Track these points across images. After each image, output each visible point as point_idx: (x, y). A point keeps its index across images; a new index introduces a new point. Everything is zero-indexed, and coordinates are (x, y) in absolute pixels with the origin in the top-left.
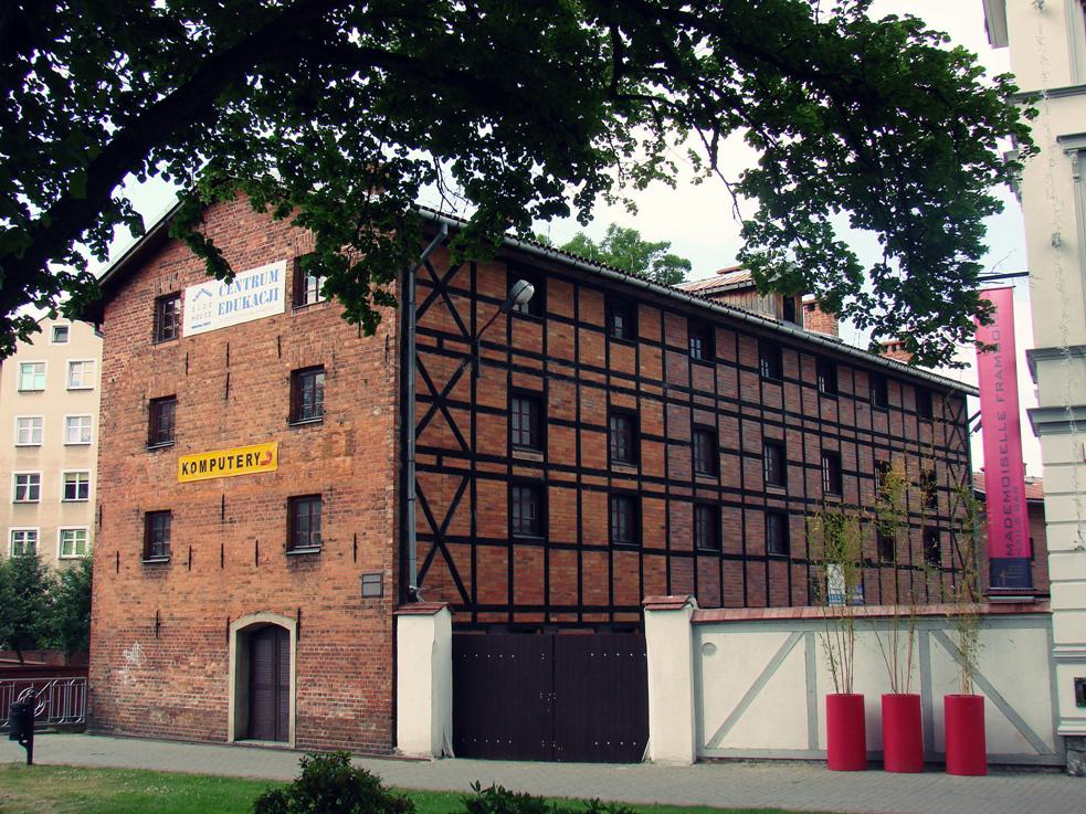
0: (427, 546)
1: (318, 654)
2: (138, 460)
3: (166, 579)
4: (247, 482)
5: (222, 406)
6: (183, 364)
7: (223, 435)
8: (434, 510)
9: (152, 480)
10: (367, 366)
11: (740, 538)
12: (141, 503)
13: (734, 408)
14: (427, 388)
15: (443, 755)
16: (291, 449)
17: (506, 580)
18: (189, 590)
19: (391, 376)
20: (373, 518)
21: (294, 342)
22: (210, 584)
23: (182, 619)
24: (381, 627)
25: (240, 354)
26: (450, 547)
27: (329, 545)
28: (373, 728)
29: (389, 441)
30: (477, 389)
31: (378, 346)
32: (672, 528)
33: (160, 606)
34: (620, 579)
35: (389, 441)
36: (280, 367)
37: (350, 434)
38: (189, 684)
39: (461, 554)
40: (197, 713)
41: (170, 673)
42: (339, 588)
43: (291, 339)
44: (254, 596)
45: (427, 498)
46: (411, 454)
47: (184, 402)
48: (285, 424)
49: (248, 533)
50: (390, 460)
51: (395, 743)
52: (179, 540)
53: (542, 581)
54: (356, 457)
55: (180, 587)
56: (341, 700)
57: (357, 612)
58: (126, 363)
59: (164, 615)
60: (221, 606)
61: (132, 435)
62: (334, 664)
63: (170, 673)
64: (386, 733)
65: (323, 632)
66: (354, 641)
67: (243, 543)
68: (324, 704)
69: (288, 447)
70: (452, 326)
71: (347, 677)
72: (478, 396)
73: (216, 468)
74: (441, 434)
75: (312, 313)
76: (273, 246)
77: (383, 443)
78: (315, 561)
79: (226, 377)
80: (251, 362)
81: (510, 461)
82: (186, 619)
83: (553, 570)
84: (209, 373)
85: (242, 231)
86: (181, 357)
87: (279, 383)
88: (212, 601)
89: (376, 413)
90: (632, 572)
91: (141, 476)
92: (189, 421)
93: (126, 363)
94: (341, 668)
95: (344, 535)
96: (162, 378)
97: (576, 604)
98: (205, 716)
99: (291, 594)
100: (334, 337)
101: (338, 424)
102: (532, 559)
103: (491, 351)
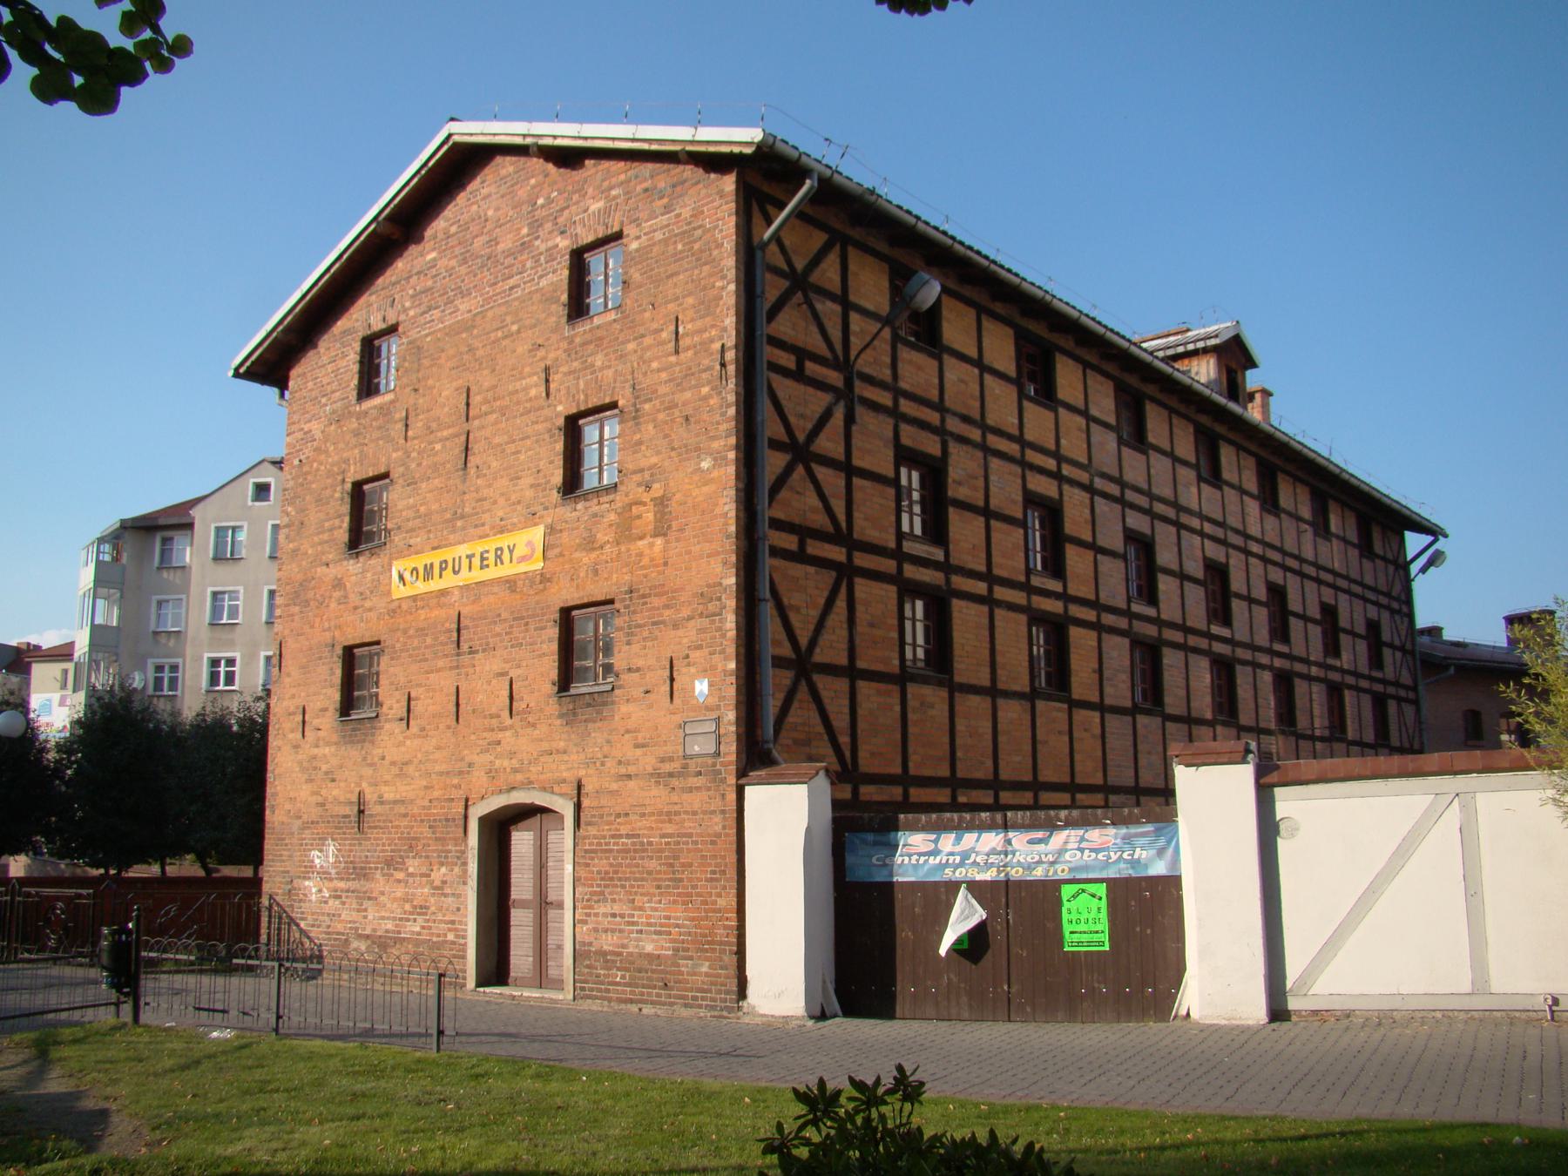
0: (786, 677)
1: (611, 851)
2: (333, 571)
3: (373, 742)
4: (496, 589)
5: (458, 481)
6: (400, 426)
7: (459, 523)
8: (795, 620)
9: (354, 599)
10: (688, 395)
11: (1183, 693)
12: (337, 633)
13: (1001, 593)
14: (782, 430)
15: (822, 1016)
16: (565, 534)
17: (898, 736)
18: (407, 757)
19: (728, 406)
20: (701, 631)
21: (570, 373)
22: (438, 748)
23: (395, 802)
24: (716, 804)
25: (486, 401)
26: (821, 681)
27: (626, 678)
28: (704, 969)
29: (727, 508)
30: (854, 441)
31: (706, 362)
32: (1106, 674)
33: (364, 785)
34: (1046, 742)
35: (728, 507)
36: (547, 412)
37: (661, 502)
38: (406, 900)
39: (833, 690)
40: (418, 943)
41: (379, 883)
42: (643, 746)
43: (564, 369)
44: (506, 763)
45: (785, 601)
46: (764, 527)
47: (401, 481)
48: (555, 496)
49: (497, 665)
50: (728, 537)
51: (742, 993)
52: (392, 684)
53: (946, 739)
54: (672, 535)
55: (393, 754)
56: (649, 924)
57: (675, 782)
58: (318, 435)
59: (370, 796)
60: (455, 781)
61: (326, 536)
62: (637, 866)
63: (379, 883)
64: (727, 977)
65: (618, 815)
66: (669, 828)
67: (489, 683)
68: (621, 931)
69: (561, 531)
70: (815, 343)
71: (659, 887)
72: (855, 453)
73: (448, 572)
74: (801, 503)
75: (598, 327)
76: (537, 238)
77: (717, 511)
78: (605, 704)
79: (463, 438)
80: (503, 411)
81: (899, 555)
82: (403, 802)
83: (960, 726)
84: (439, 434)
85: (489, 226)
86: (397, 416)
87: (547, 436)
88: (441, 774)
89: (705, 465)
90: (1059, 732)
91: (337, 594)
92: (409, 508)
93: (318, 435)
94: (650, 873)
95: (652, 661)
96: (370, 450)
97: (991, 777)
98: (431, 948)
99: (565, 757)
100: (634, 358)
101: (641, 489)
102: (932, 706)
103: (871, 388)
